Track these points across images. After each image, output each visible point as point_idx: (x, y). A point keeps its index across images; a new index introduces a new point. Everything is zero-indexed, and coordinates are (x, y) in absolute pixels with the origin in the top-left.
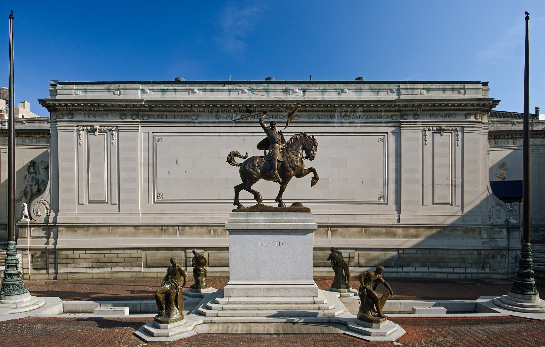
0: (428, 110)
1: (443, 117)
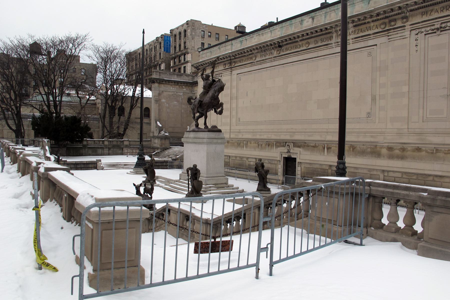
0: (418, 9)
1: (439, 12)
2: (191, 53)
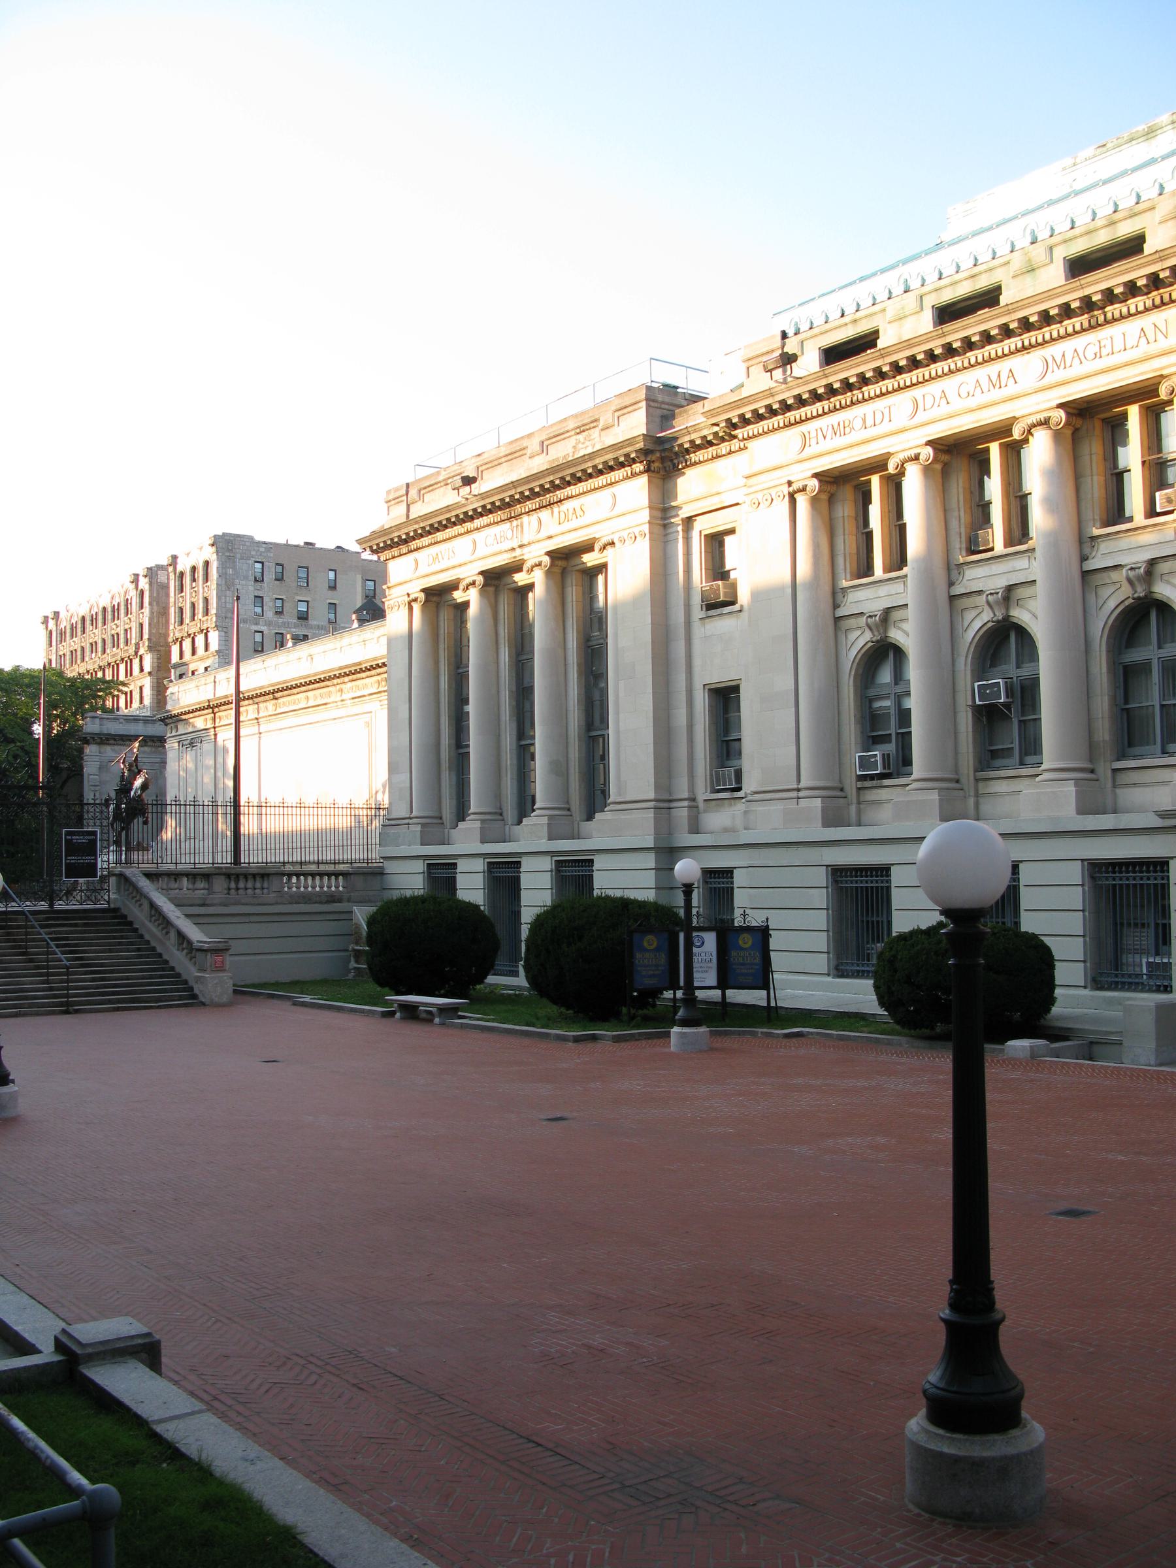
2: (225, 630)
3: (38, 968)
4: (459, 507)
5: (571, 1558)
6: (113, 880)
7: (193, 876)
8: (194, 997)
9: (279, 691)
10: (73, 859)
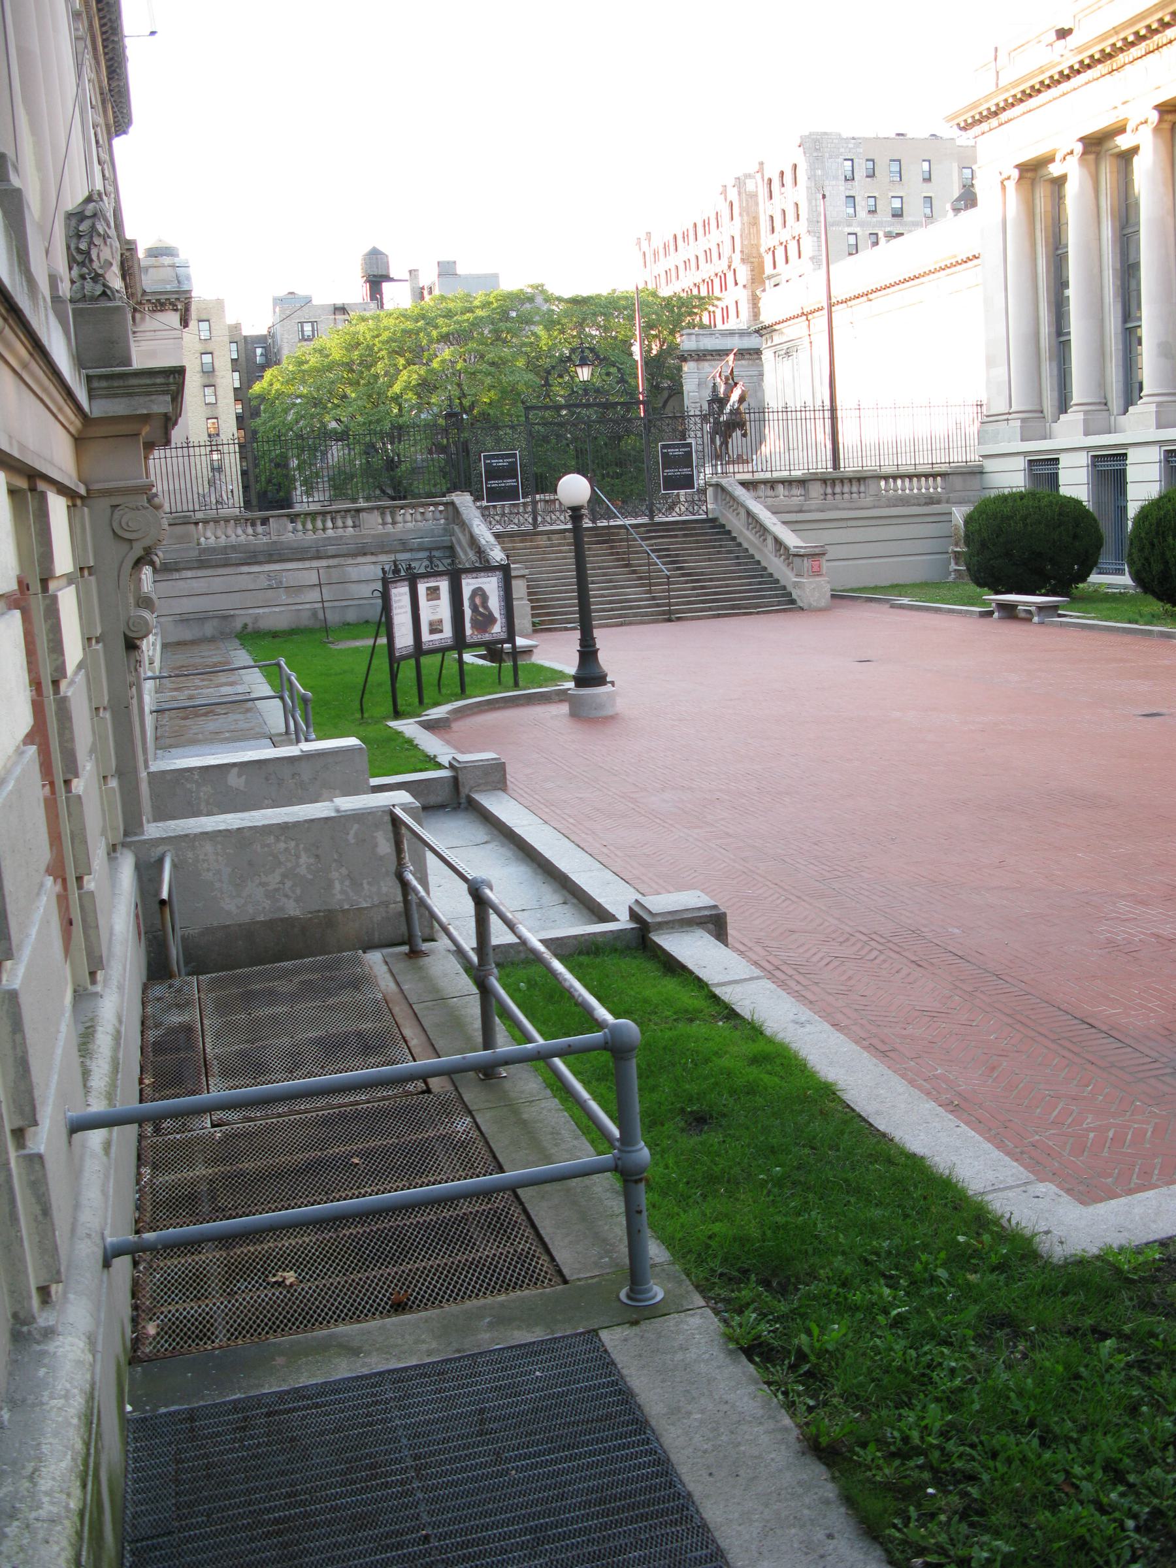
3: (641, 578)
4: (1054, 66)
5: (1111, 1134)
6: (710, 491)
7: (788, 482)
8: (793, 602)
9: (873, 292)
10: (670, 472)
